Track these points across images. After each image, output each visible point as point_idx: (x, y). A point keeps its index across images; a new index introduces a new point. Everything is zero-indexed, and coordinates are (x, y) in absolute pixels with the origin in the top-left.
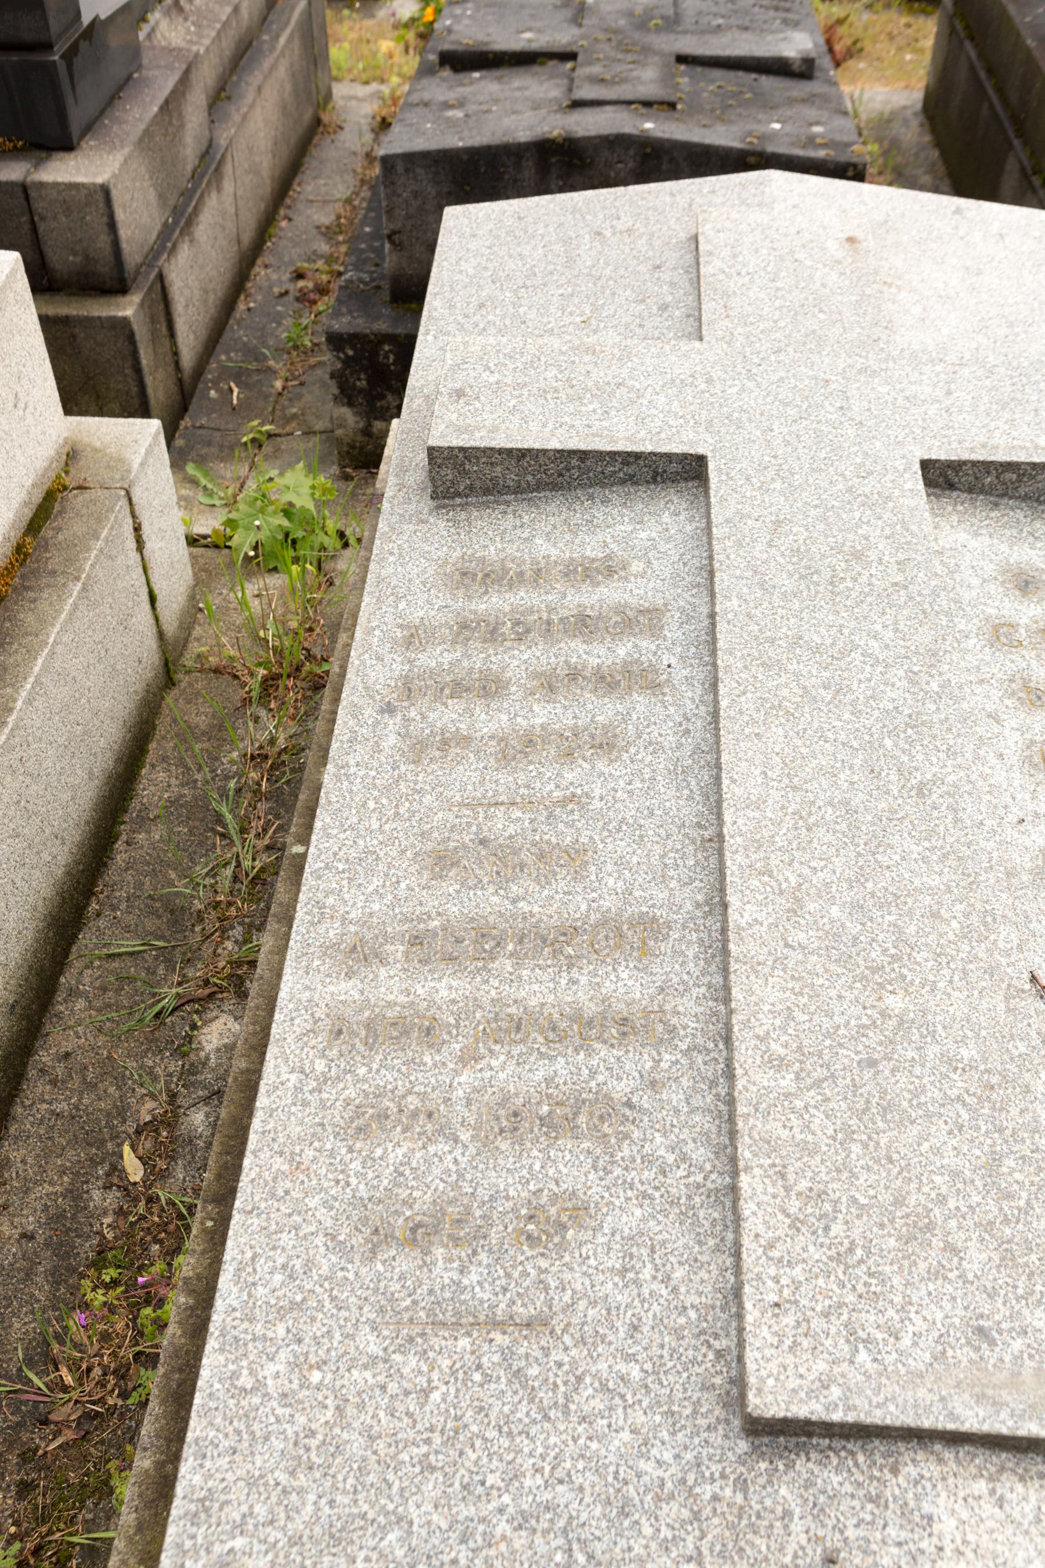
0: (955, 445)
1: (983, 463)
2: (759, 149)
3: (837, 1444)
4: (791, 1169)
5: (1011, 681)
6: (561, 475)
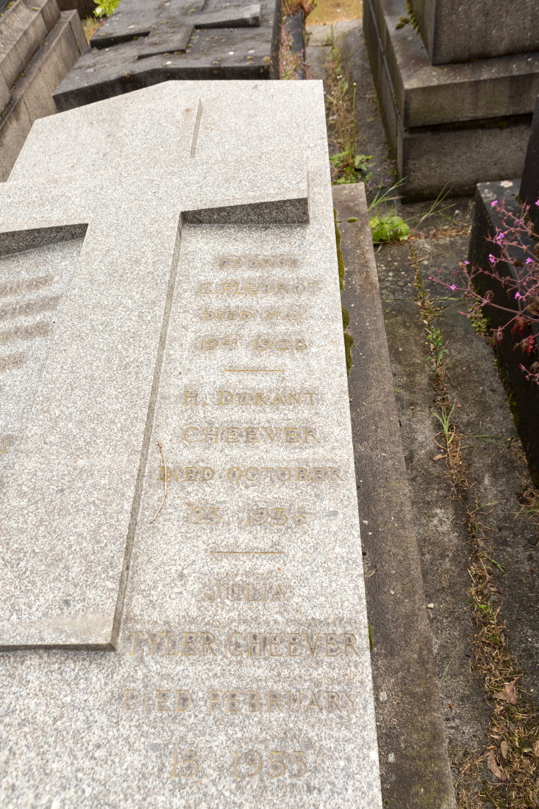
0: (198, 203)
1: (209, 209)
2: (218, 66)
3: (5, 654)
4: (12, 540)
5: (199, 309)
6: (33, 241)
